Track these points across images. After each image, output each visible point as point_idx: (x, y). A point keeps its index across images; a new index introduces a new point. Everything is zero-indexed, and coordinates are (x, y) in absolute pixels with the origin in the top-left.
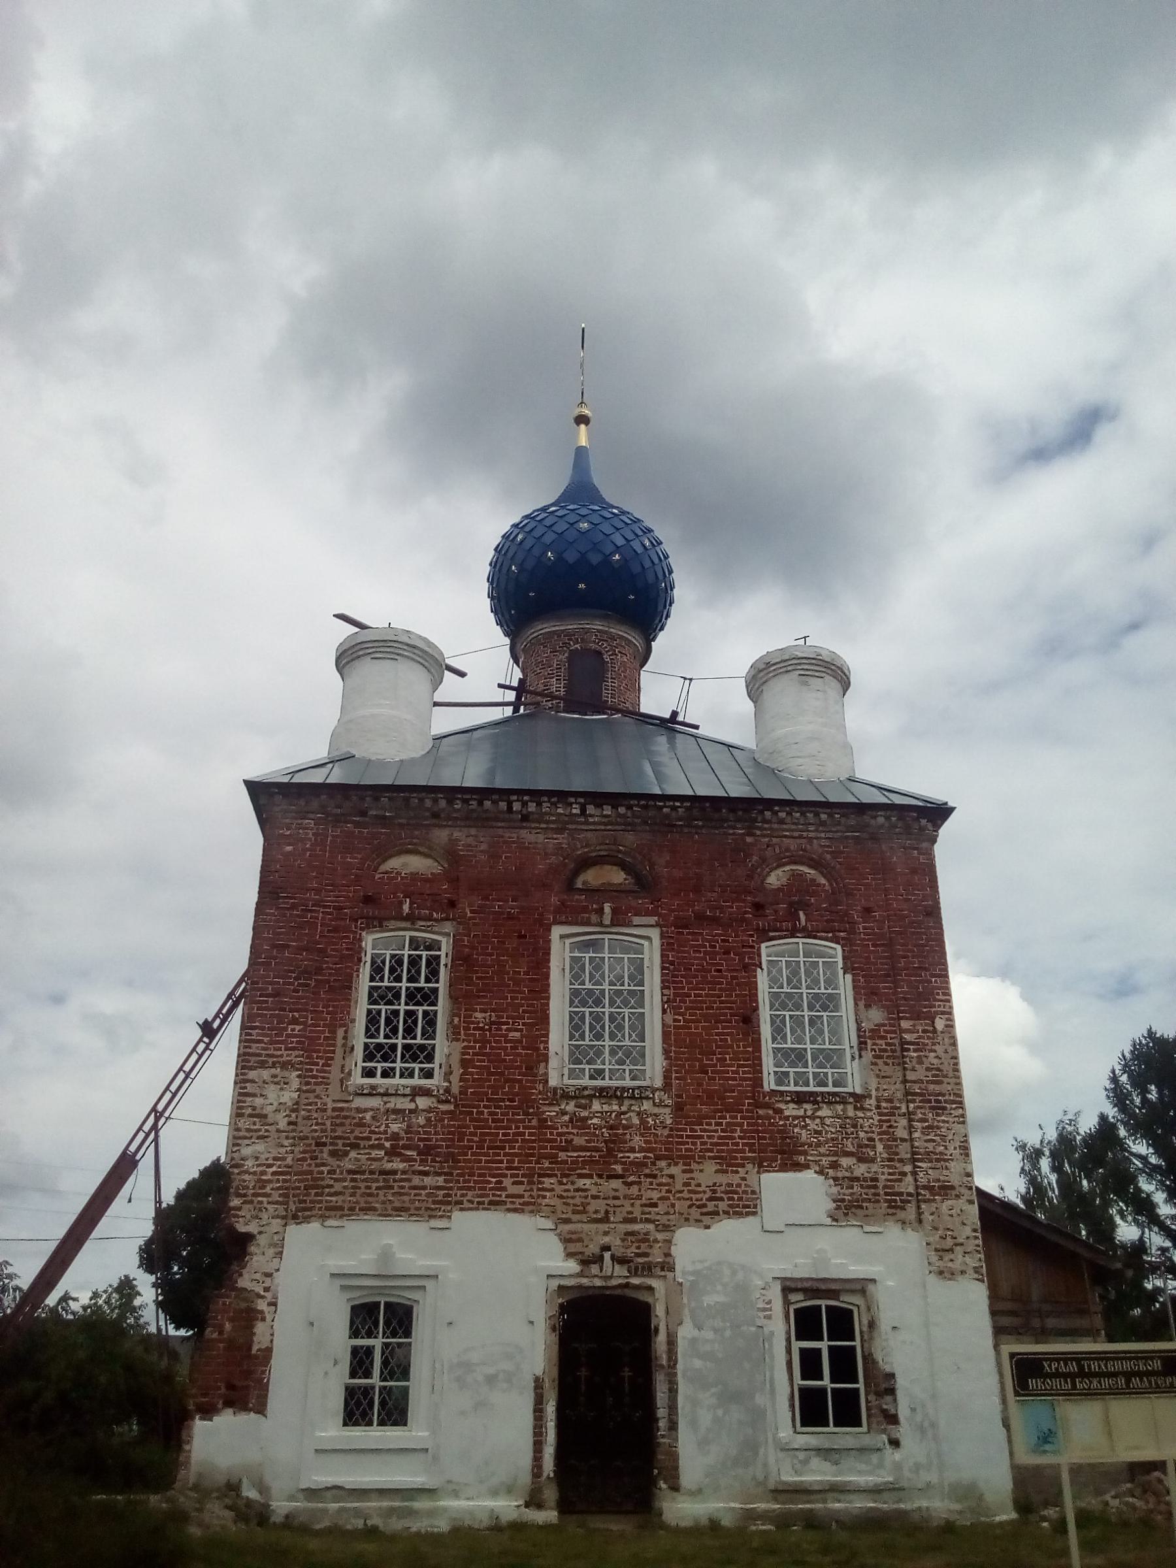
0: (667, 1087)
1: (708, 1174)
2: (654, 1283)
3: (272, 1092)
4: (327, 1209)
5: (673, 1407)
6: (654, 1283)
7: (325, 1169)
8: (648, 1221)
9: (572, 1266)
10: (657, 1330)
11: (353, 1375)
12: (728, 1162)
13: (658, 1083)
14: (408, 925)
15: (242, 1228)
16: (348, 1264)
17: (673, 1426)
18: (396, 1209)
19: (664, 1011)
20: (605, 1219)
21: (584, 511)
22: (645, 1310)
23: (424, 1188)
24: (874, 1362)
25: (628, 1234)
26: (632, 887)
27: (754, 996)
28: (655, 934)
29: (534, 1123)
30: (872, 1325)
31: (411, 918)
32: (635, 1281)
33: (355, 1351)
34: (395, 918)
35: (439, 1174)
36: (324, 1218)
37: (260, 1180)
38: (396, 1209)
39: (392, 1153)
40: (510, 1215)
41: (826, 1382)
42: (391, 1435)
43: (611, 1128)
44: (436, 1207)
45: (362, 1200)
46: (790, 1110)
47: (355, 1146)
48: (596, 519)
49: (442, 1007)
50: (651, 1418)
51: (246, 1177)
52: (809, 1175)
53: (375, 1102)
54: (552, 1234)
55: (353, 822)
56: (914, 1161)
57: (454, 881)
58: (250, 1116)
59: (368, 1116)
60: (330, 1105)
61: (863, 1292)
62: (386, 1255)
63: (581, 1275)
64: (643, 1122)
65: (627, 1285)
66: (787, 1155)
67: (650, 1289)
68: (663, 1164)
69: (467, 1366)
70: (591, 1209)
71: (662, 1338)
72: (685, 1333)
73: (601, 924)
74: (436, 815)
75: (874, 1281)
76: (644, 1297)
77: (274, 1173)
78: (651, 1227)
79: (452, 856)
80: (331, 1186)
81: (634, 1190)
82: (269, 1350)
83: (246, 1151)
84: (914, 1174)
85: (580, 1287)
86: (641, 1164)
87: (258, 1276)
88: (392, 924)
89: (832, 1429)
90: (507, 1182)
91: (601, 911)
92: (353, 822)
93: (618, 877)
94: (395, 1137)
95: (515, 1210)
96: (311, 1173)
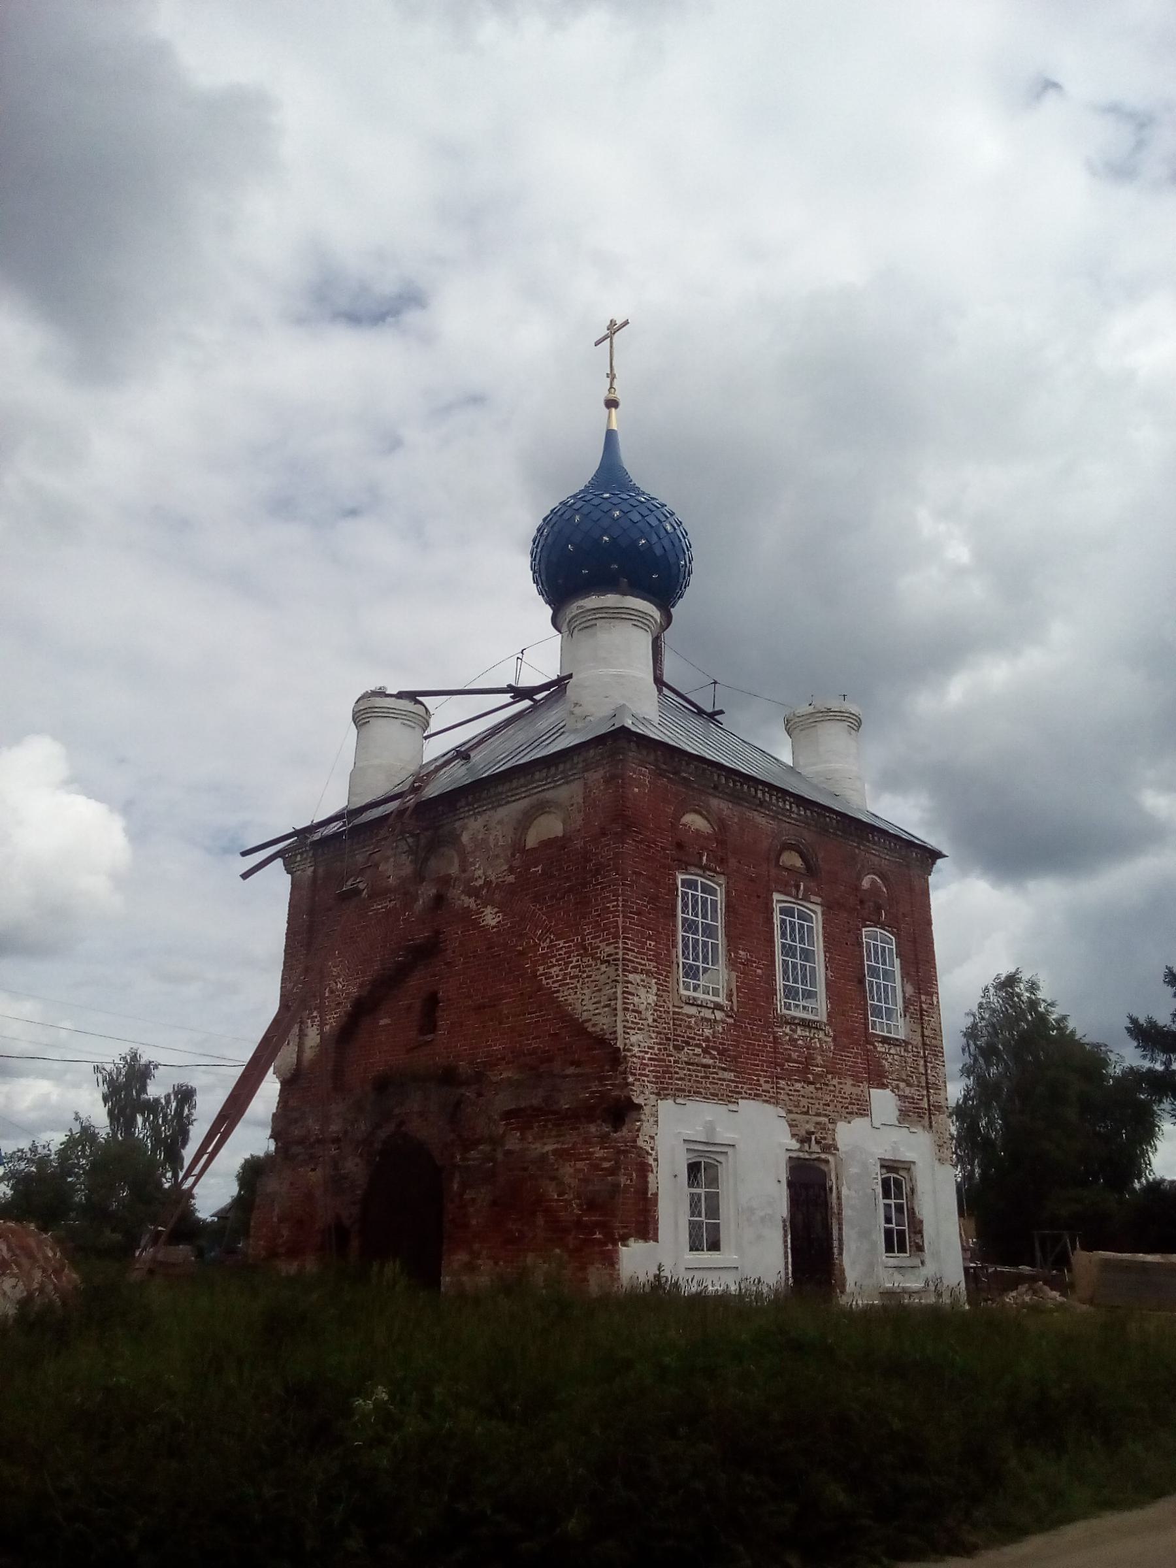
0: (830, 1023)
1: (848, 1087)
2: (830, 1158)
3: (642, 992)
4: (677, 1090)
5: (840, 1240)
6: (830, 1158)
7: (672, 1059)
8: (826, 1115)
9: (794, 1144)
10: (831, 1189)
11: (692, 1215)
12: (857, 1080)
13: (825, 1020)
14: (700, 872)
15: (636, 1101)
16: (690, 1133)
17: (841, 1254)
18: (712, 1094)
19: (827, 968)
20: (807, 1113)
21: (616, 500)
22: (824, 1175)
23: (724, 1080)
24: (914, 1213)
25: (817, 1123)
26: (803, 871)
27: (727, 935)
28: (819, 909)
29: (771, 1039)
30: (913, 1190)
31: (705, 868)
32: (823, 1156)
33: (692, 1195)
34: (696, 866)
35: (732, 1071)
36: (675, 1097)
37: (642, 1064)
38: (712, 1094)
39: (706, 1051)
40: (766, 1105)
41: (893, 1226)
42: (714, 1255)
43: (808, 1049)
44: (729, 1097)
45: (695, 1085)
46: (880, 1048)
47: (688, 1044)
48: (626, 508)
49: (721, 941)
50: (830, 1247)
51: (635, 1060)
52: (888, 1091)
53: (692, 1010)
54: (784, 1120)
55: (668, 778)
56: (928, 1088)
57: (722, 843)
58: (633, 1011)
59: (693, 1020)
60: (671, 1009)
61: (909, 1169)
62: (710, 1128)
63: (800, 1150)
64: (821, 1046)
65: (818, 1159)
66: (878, 1078)
67: (827, 1162)
68: (830, 1076)
69: (752, 1210)
70: (801, 1104)
71: (834, 1194)
72: (845, 1191)
73: (797, 898)
74: (715, 788)
75: (914, 1163)
76: (823, 1167)
77: (650, 1059)
78: (826, 1120)
79: (722, 825)
80: (677, 1073)
81: (819, 1094)
82: (656, 1194)
83: (633, 1039)
84: (928, 1096)
85: (799, 1158)
86: (821, 1076)
87: (647, 1138)
88: (693, 869)
89: (896, 1254)
90: (762, 1080)
91: (797, 887)
92: (668, 778)
93: (799, 863)
94: (707, 1040)
95: (766, 1101)
96: (664, 1061)
